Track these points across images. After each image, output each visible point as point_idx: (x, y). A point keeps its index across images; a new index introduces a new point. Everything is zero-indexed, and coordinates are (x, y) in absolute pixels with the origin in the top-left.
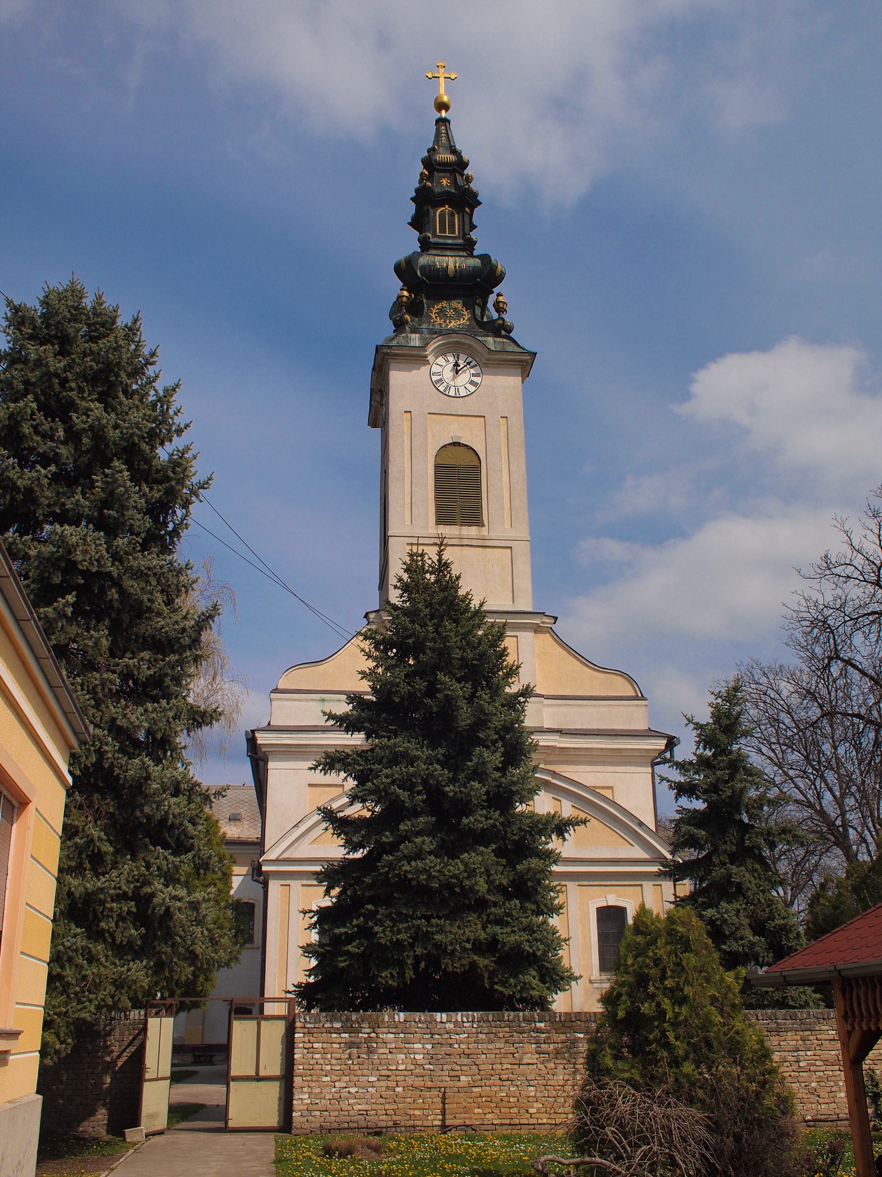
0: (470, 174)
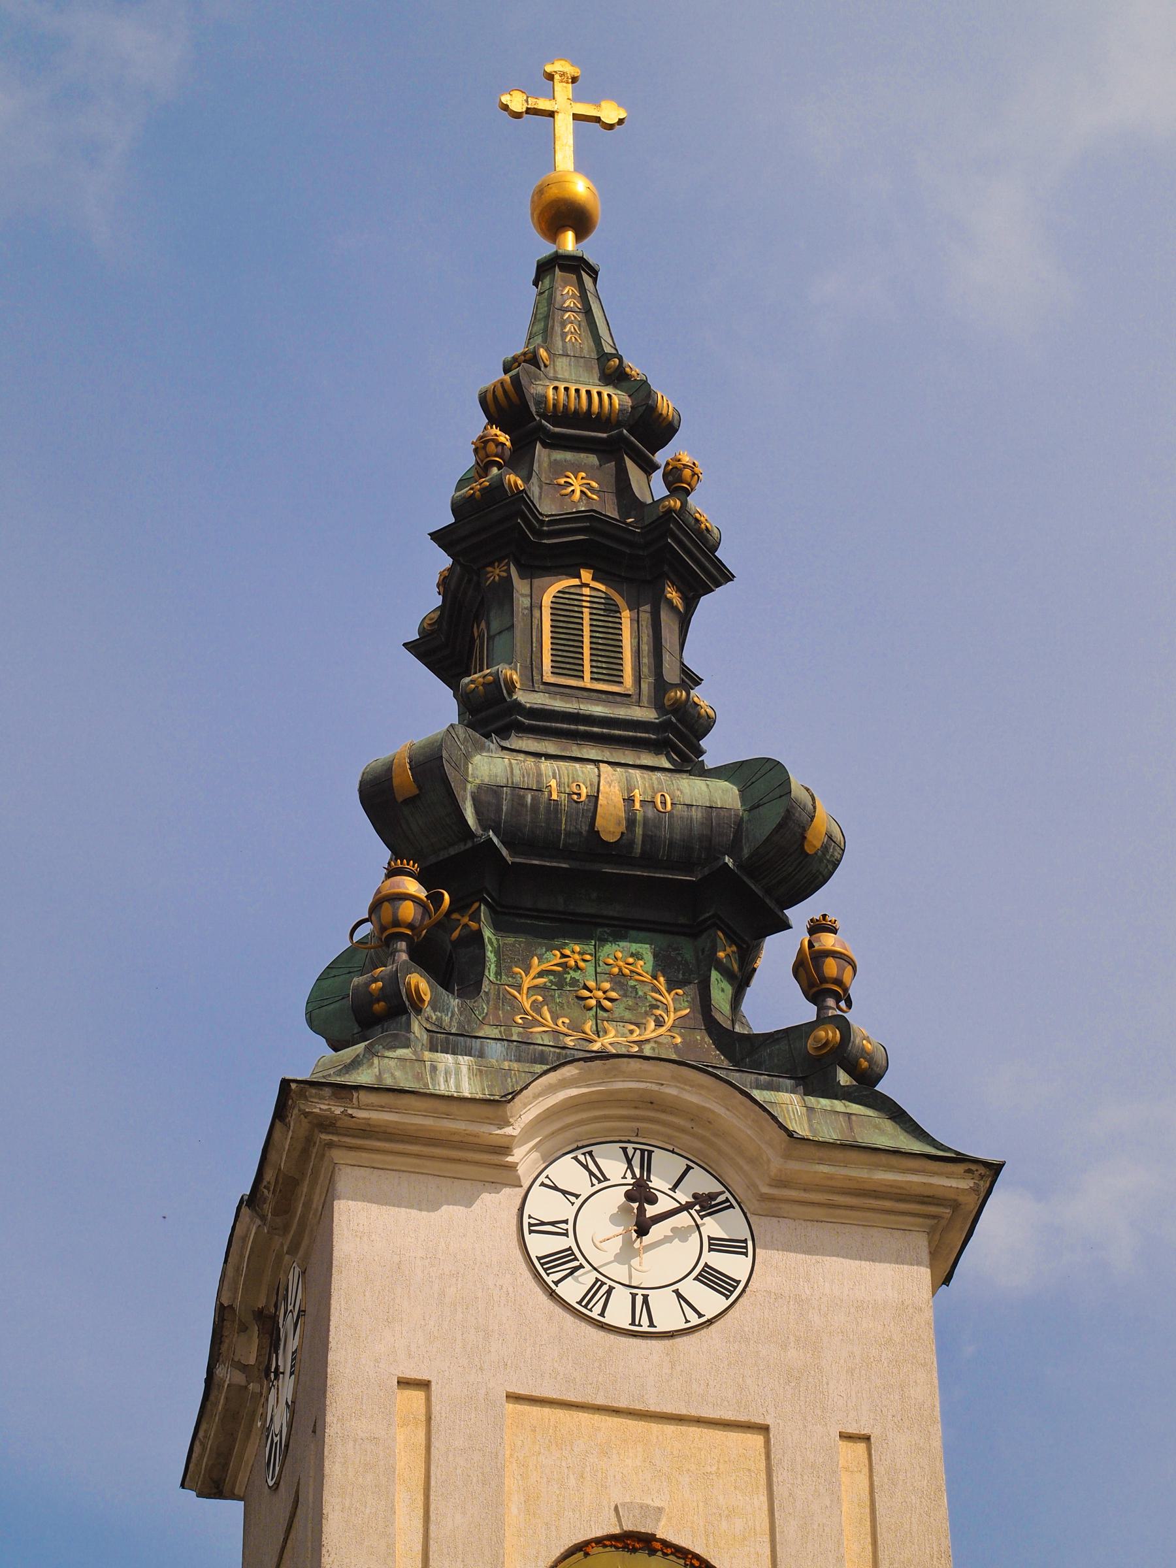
0: (686, 459)
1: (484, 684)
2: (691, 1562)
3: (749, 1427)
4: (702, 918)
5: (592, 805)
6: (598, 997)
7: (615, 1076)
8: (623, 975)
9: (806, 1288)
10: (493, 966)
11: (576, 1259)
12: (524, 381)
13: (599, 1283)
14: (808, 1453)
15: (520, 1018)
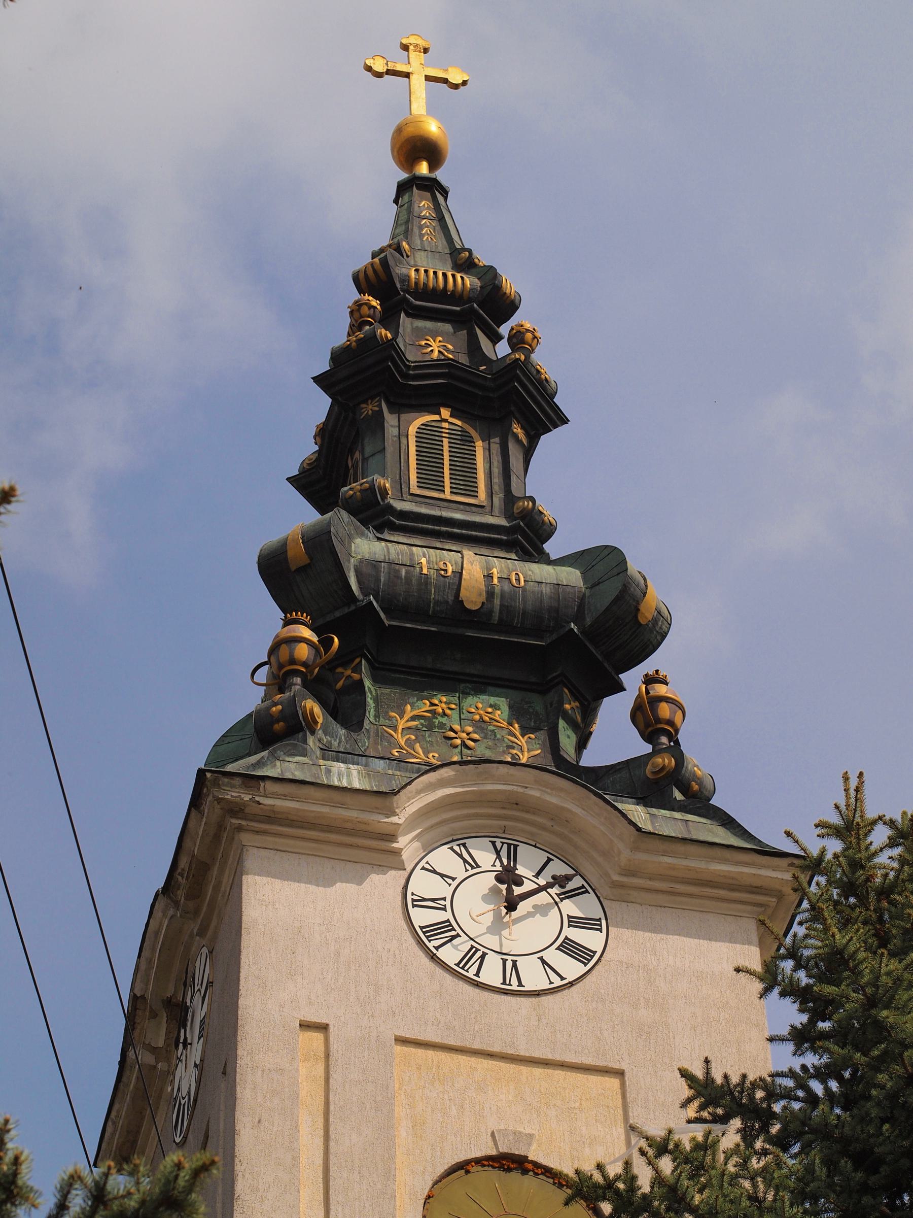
0: (528, 326)
1: (361, 491)
2: (559, 1181)
3: (607, 1072)
4: (549, 678)
5: (457, 579)
6: (462, 737)
7: (486, 779)
8: (483, 721)
9: (653, 960)
10: (372, 710)
11: (453, 929)
12: (391, 262)
13: (474, 949)
14: (659, 1093)
15: (397, 752)
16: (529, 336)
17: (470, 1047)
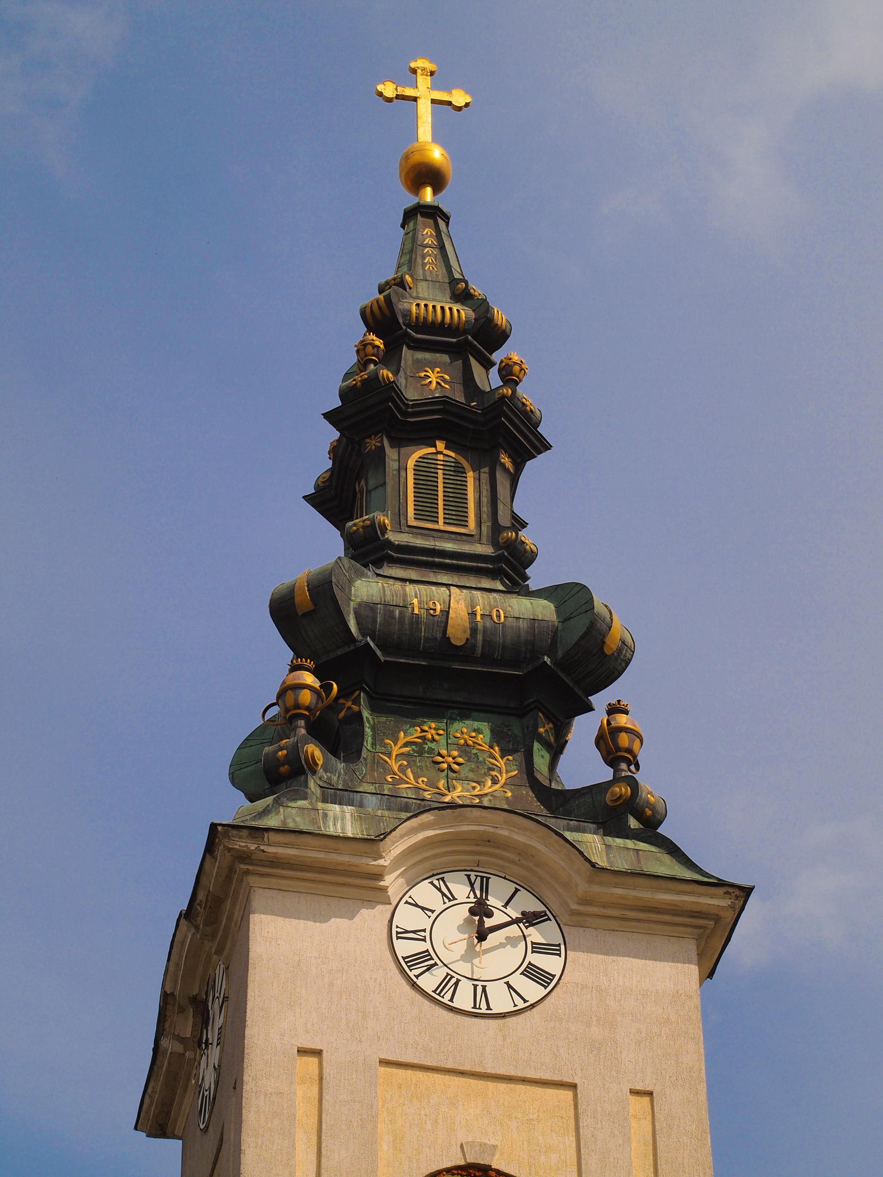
0: (516, 358)
1: (363, 527)
3: (562, 1085)
4: (526, 703)
5: (444, 617)
7: (461, 821)
8: (468, 745)
9: (605, 981)
11: (432, 959)
12: (394, 299)
13: (449, 976)
14: (606, 1104)
15: (390, 778)
16: (516, 368)
17: (444, 1066)
